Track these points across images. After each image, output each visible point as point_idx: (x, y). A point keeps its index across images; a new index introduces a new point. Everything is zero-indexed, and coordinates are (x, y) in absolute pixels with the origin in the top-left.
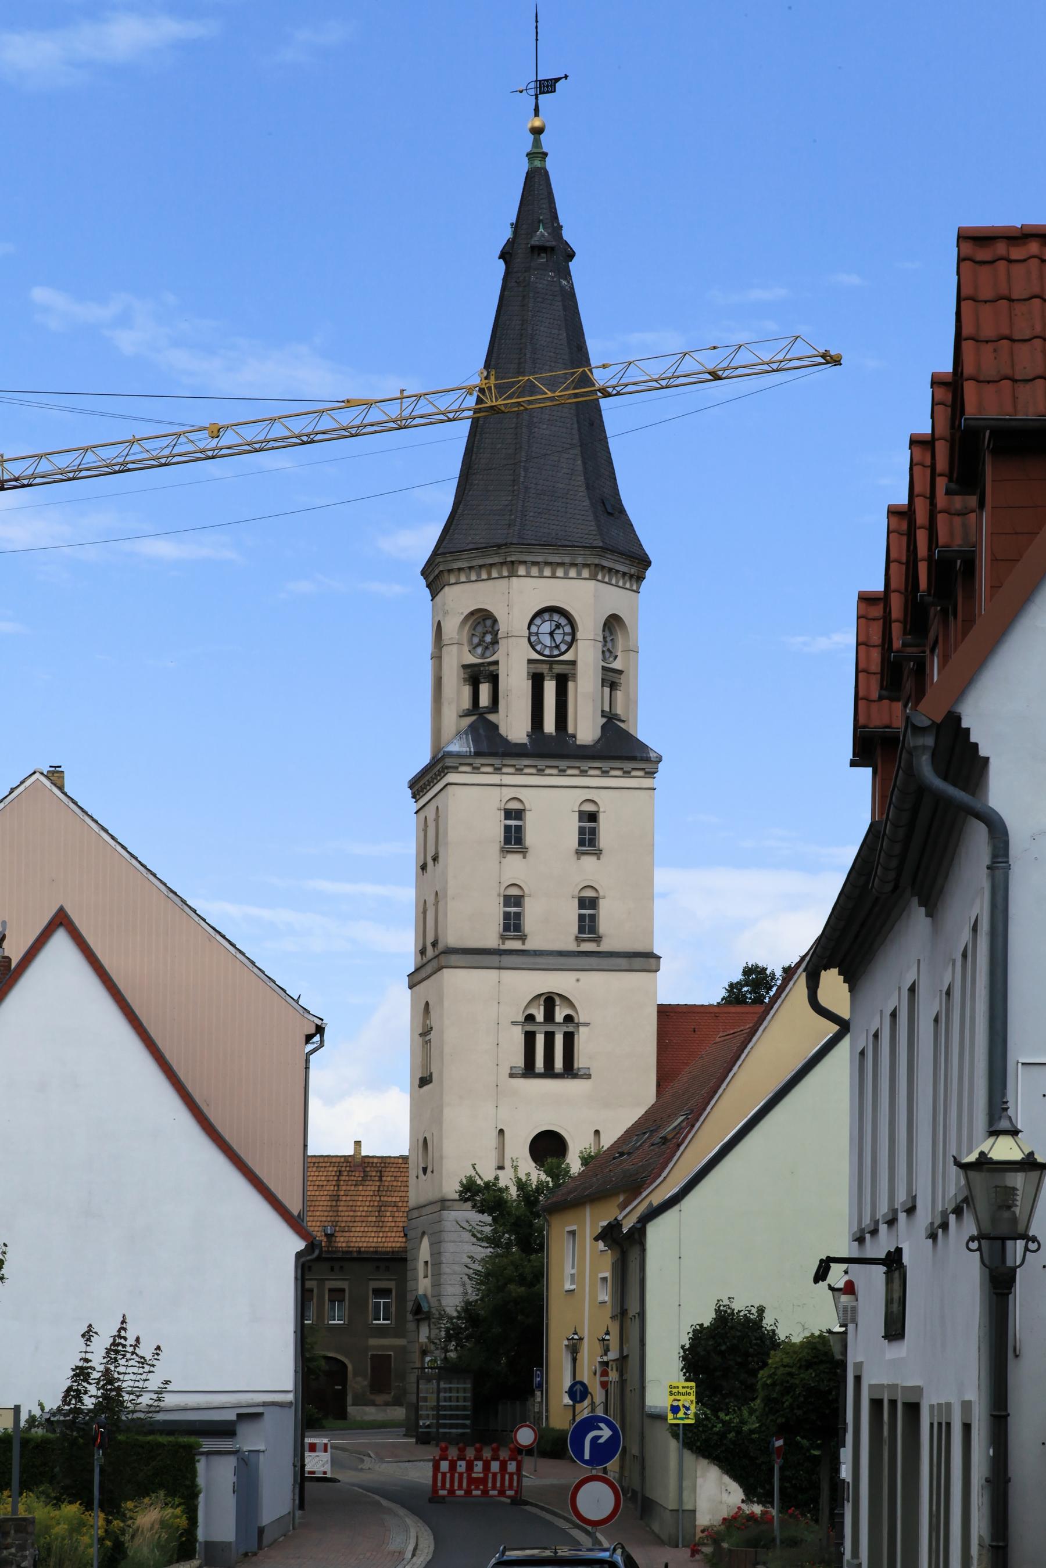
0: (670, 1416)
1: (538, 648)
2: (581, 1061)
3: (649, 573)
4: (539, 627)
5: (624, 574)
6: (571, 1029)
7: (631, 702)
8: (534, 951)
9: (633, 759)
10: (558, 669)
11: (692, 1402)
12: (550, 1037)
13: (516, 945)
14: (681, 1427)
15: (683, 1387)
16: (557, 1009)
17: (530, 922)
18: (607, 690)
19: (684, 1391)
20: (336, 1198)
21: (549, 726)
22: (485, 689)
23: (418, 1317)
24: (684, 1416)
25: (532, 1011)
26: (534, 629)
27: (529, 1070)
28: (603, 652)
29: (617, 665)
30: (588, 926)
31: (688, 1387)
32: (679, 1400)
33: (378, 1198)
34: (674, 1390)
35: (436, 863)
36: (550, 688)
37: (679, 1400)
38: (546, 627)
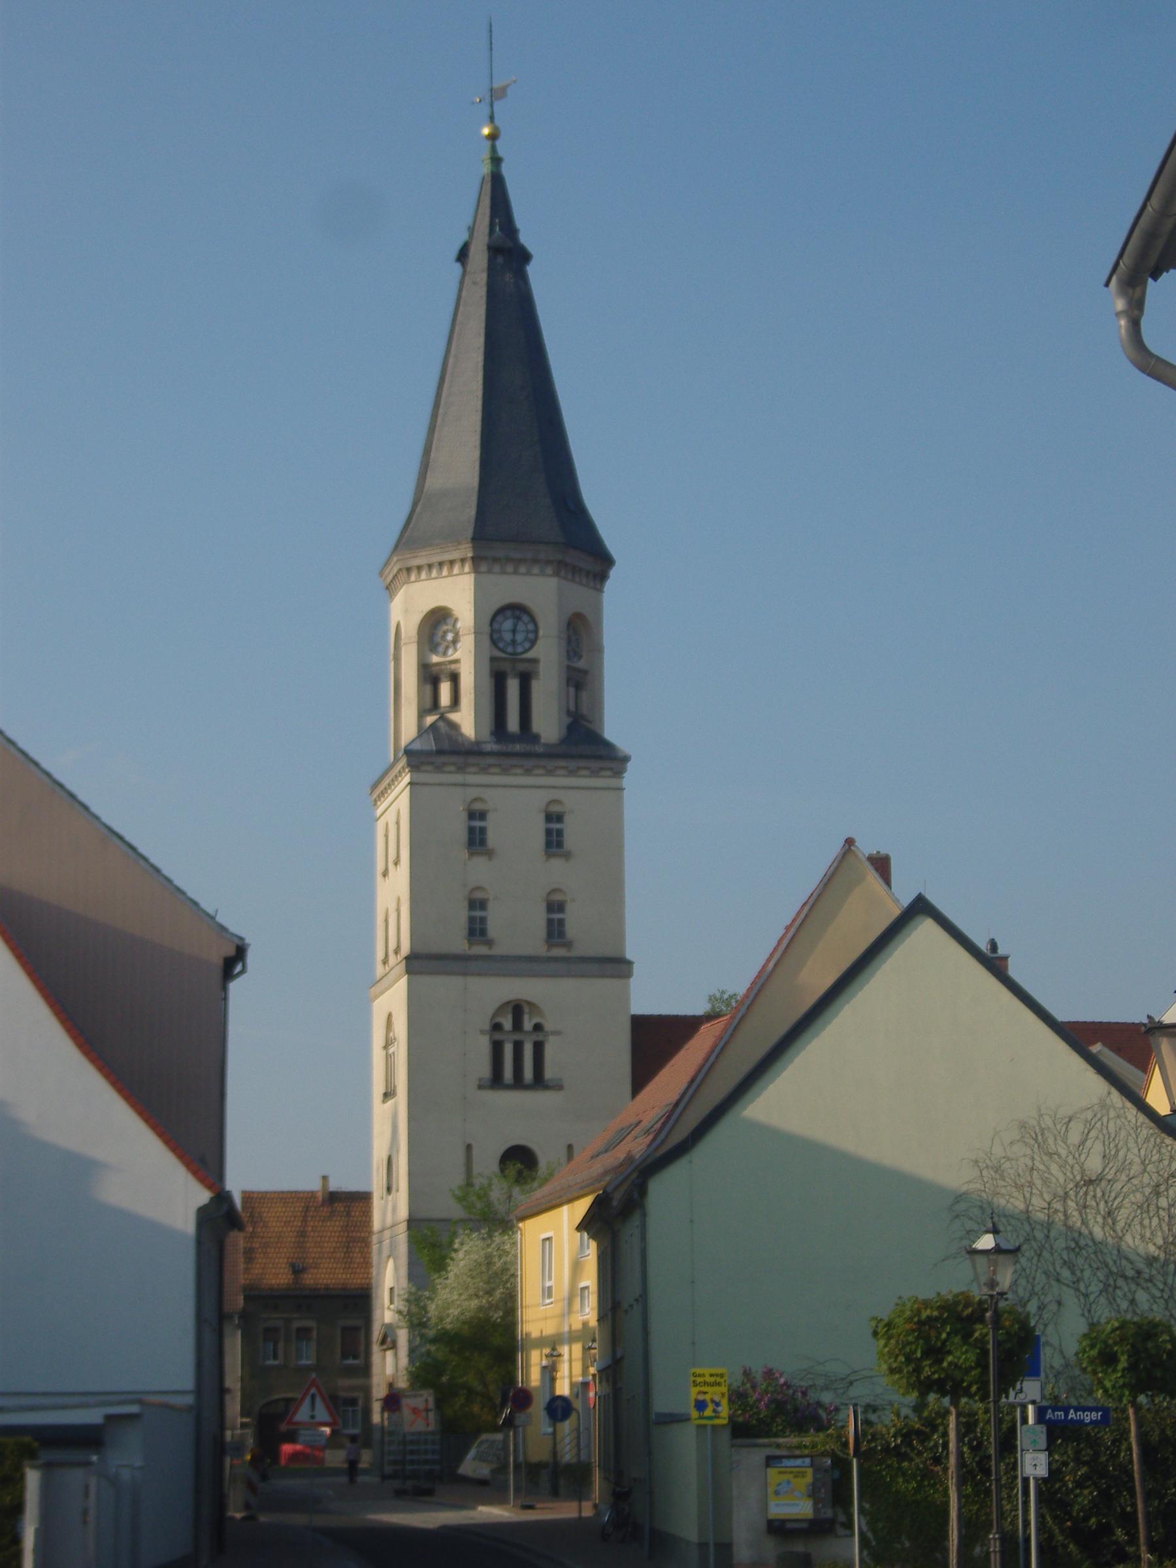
0: (694, 1414)
1: (501, 645)
2: (549, 1073)
3: (613, 573)
4: (501, 624)
5: (588, 573)
6: (540, 1037)
7: (597, 704)
8: (502, 957)
9: (600, 758)
10: (522, 667)
11: (723, 1395)
12: (518, 1047)
13: (482, 950)
14: (709, 1428)
15: (711, 1375)
16: (526, 1018)
17: (494, 928)
18: (572, 690)
19: (712, 1379)
20: (302, 1234)
21: (513, 723)
22: (445, 689)
23: (385, 1347)
24: (713, 1414)
25: (499, 1019)
26: (496, 626)
27: (496, 1081)
28: (568, 651)
29: (581, 664)
30: (555, 931)
31: (717, 1375)
32: (705, 1393)
33: (346, 1234)
34: (699, 1380)
35: (398, 866)
36: (513, 687)
37: (705, 1393)
38: (508, 625)
